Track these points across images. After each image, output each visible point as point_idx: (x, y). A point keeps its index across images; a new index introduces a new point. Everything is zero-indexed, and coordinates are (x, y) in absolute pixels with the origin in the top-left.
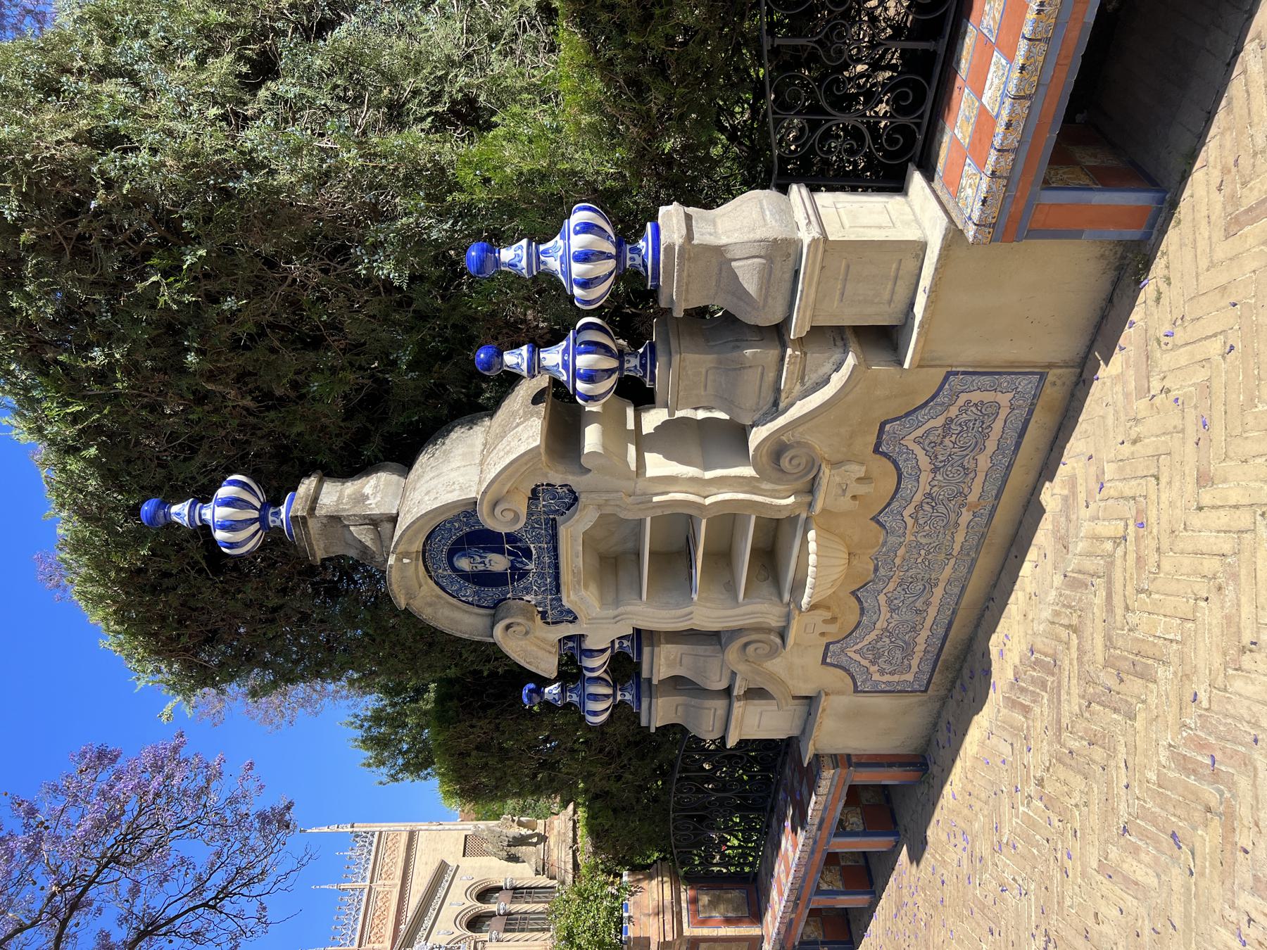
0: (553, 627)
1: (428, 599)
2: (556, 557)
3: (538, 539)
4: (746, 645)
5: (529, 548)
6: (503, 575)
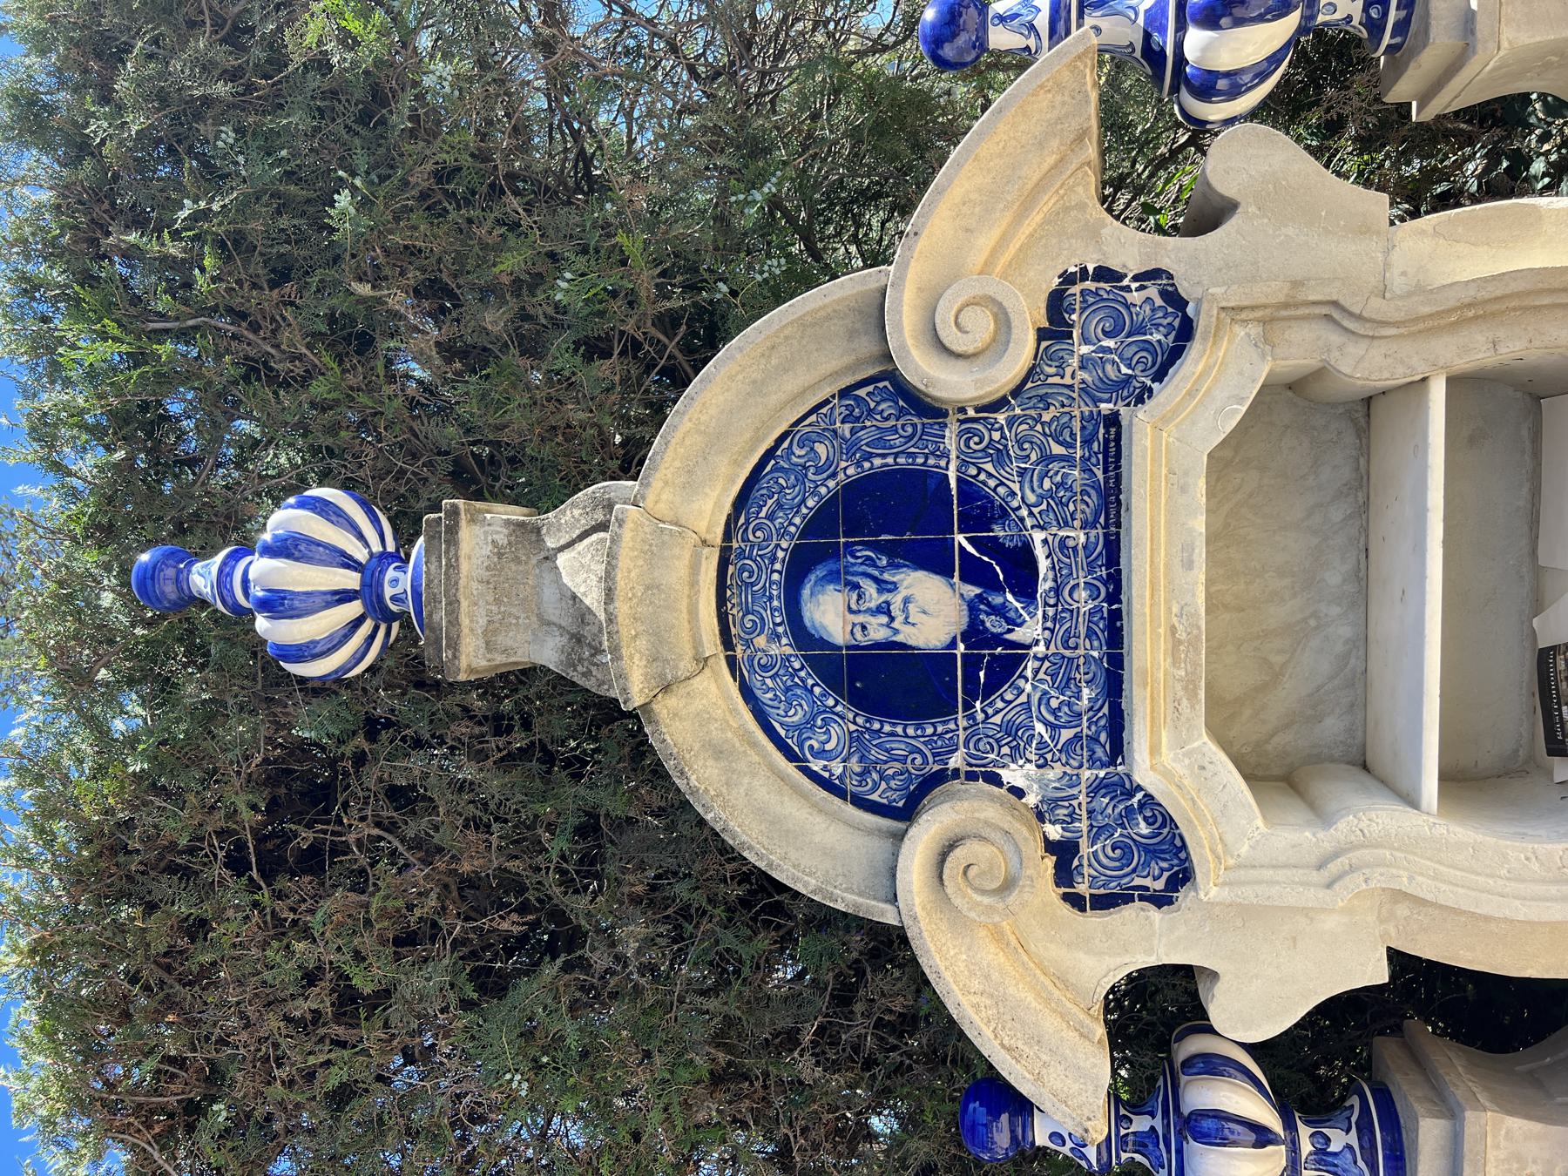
0: (1094, 920)
2: (1114, 586)
3: (1056, 507)
5: (1027, 549)
6: (939, 662)
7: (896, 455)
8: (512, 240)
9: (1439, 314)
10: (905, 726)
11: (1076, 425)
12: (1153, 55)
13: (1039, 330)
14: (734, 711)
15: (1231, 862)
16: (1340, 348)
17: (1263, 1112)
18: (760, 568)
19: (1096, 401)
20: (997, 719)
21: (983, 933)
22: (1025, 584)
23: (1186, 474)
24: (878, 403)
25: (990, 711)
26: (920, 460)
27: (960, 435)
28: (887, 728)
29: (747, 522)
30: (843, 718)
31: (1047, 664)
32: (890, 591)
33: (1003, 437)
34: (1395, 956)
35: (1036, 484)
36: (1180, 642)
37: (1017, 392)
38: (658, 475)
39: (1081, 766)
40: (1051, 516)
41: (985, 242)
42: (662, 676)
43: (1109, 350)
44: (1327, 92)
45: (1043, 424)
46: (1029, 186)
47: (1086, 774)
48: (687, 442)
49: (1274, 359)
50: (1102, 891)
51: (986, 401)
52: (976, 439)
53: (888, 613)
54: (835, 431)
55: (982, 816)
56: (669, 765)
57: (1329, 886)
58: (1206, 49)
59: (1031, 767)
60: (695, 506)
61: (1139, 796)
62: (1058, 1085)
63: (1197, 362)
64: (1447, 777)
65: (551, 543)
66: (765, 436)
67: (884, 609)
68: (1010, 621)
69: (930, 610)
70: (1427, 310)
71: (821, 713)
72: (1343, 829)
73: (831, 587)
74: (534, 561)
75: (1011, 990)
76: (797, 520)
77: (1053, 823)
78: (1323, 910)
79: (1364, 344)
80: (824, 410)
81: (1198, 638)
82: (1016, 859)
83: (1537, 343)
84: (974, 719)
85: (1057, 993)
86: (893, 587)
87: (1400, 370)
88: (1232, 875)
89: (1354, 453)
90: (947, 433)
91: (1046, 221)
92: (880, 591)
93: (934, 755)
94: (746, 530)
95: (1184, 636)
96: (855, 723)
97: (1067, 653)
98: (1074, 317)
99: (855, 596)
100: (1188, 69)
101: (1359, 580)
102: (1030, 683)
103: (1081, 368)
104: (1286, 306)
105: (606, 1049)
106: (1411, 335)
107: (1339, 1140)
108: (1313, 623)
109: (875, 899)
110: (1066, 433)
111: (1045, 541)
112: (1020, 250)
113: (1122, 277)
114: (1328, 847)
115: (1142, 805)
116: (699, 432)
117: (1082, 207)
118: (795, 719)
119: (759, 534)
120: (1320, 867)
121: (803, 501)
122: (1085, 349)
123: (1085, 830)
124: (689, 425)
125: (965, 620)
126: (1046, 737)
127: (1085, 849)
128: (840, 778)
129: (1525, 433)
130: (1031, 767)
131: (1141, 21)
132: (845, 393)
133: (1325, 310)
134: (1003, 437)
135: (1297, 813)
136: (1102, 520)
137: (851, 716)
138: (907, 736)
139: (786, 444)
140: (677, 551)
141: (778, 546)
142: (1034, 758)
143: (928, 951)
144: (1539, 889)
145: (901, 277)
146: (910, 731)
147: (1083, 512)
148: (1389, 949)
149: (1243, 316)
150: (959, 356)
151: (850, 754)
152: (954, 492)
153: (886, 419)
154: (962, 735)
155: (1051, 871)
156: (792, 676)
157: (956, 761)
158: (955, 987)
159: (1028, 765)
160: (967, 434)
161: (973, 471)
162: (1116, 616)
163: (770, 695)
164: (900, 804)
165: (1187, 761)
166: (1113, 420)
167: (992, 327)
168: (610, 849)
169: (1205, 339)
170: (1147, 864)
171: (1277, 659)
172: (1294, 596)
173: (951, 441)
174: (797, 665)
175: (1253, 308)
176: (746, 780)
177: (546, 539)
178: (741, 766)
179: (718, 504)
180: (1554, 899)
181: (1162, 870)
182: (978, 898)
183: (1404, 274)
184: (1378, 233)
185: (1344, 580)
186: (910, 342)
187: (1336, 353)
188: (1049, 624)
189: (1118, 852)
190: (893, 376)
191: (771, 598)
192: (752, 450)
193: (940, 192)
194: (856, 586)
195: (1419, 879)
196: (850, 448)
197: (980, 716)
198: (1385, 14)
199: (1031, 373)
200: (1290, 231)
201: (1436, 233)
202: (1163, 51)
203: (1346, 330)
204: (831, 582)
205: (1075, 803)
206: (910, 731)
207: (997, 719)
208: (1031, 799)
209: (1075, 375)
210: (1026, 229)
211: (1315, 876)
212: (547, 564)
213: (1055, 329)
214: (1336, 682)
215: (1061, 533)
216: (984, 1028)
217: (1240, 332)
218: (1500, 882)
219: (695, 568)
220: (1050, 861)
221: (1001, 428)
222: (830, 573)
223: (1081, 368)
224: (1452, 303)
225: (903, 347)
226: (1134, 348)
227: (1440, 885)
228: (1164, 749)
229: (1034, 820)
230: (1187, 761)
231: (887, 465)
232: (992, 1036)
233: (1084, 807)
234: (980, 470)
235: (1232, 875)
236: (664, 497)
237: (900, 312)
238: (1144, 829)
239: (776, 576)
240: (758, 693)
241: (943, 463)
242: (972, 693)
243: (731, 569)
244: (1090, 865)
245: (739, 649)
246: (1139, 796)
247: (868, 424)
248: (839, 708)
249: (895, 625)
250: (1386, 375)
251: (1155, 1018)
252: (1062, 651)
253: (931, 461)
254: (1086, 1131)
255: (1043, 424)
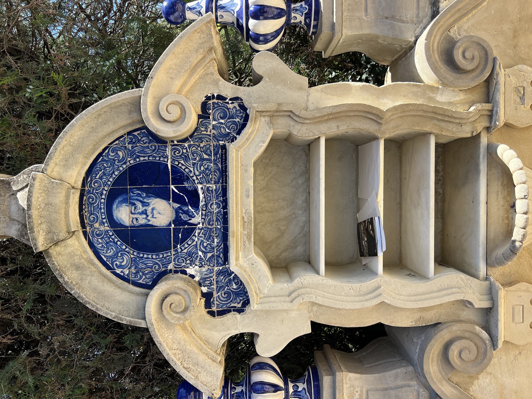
0: (218, 320)
1: (76, 260)
2: (225, 204)
3: (205, 177)
4: (447, 347)
5: (196, 191)
6: (165, 231)
7: (149, 157)
8: (9, 73)
9: (322, 117)
10: (152, 255)
11: (212, 149)
12: (240, 26)
13: (199, 115)
14: (85, 252)
15: (262, 296)
16: (293, 126)
17: (277, 381)
18: (96, 198)
19: (218, 141)
20: (185, 251)
21: (178, 327)
22: (195, 203)
23: (247, 166)
24: (142, 138)
25: (183, 248)
26: (158, 159)
27: (172, 150)
28: (145, 256)
29: (91, 180)
30: (128, 253)
31: (203, 231)
32: (147, 206)
33: (187, 151)
34: (313, 324)
35: (198, 168)
36: (245, 222)
37: (191, 136)
38: (52, 161)
39: (214, 266)
40: (204, 179)
41: (178, 83)
42: (52, 239)
43: (222, 123)
44: (299, 47)
45: (201, 147)
46: (193, 65)
47: (216, 268)
48: (65, 149)
49: (273, 129)
50: (221, 309)
51: (180, 138)
52: (178, 152)
53: (146, 214)
54: (125, 147)
55: (176, 285)
56: (56, 273)
57: (292, 302)
58: (254, 26)
59: (197, 267)
60: (69, 173)
61: (233, 275)
62: (204, 379)
63: (249, 129)
64: (328, 264)
65: (14, 188)
66: (98, 148)
67: (145, 213)
68: (190, 216)
69: (161, 213)
70: (318, 115)
71: (120, 251)
72: (297, 282)
73: (124, 204)
74: (8, 195)
75: (188, 347)
76: (111, 180)
77: (204, 287)
78: (291, 310)
79: (300, 125)
80: (121, 139)
81: (251, 220)
82: (189, 300)
83: (350, 127)
84: (177, 251)
85: (205, 347)
86: (148, 204)
87: (311, 134)
88: (262, 300)
89: (305, 162)
90: (167, 149)
91: (200, 78)
92: (143, 206)
93: (163, 265)
94: (91, 183)
95: (247, 220)
96: (133, 255)
97: (210, 227)
98: (210, 111)
99: (133, 208)
100: (250, 32)
101: (307, 202)
102: (197, 238)
103: (213, 129)
104: (277, 111)
105: (46, 385)
106: (315, 123)
107: (301, 386)
108: (293, 216)
109: (138, 318)
110: (209, 151)
111: (202, 188)
112: (192, 87)
113: (226, 99)
114: (292, 289)
115: (234, 278)
116: (70, 145)
117: (212, 74)
118: (110, 254)
119: (96, 184)
120: (289, 295)
121: (114, 172)
122: (214, 123)
123: (215, 288)
124: (65, 142)
125: (174, 216)
126: (202, 256)
127: (215, 295)
128: (128, 275)
129: (354, 156)
130: (197, 267)
131: (235, 15)
132: (129, 133)
133: (288, 114)
134: (187, 151)
135: (286, 277)
136: (221, 181)
137: (132, 252)
138: (153, 258)
139: (107, 151)
140: (59, 190)
141: (103, 189)
142: (198, 264)
143: (157, 336)
144: (353, 298)
145: (146, 94)
146: (154, 257)
147: (214, 178)
148: (311, 322)
149: (264, 114)
150: (168, 122)
151: (131, 266)
152: (170, 170)
153: (145, 143)
154: (173, 257)
155: (203, 303)
156: (109, 238)
157: (171, 267)
158: (167, 348)
159: (196, 267)
160: (174, 150)
161: (177, 163)
162: (226, 214)
163: (100, 245)
164: (150, 283)
165: (248, 262)
166: (224, 147)
167: (179, 112)
168: (49, 308)
169: (251, 121)
170: (236, 299)
171: (283, 228)
172: (288, 207)
173: (169, 152)
174: (111, 234)
175: (267, 112)
176: (89, 278)
177: (13, 187)
178: (88, 272)
179: (79, 173)
180: (357, 302)
181: (241, 300)
182: (175, 315)
183: (313, 103)
184: (305, 90)
185: (303, 202)
186: (150, 116)
187: (292, 128)
188: (203, 217)
189: (226, 295)
190: (145, 128)
191: (101, 209)
192: (93, 153)
193: (161, 64)
194: (134, 204)
195: (318, 298)
196: (131, 153)
197: (179, 250)
198: (311, 21)
199: (196, 130)
200: (279, 87)
201: (322, 91)
202: (243, 25)
203: (295, 120)
204: (124, 203)
205: (212, 279)
206: (154, 257)
207: (185, 251)
208: (197, 279)
209: (211, 131)
210: (193, 80)
211: (288, 299)
212: (13, 196)
213: (204, 115)
214: (301, 235)
215: (207, 185)
216: (177, 362)
217: (263, 119)
218: (342, 297)
219: (67, 197)
220: (203, 300)
221: (186, 148)
222: (124, 199)
223: (213, 129)
224: (325, 113)
225: (147, 117)
226: (230, 123)
227: (324, 299)
228: (240, 259)
229: (198, 286)
230: (248, 262)
231: (145, 160)
232: (180, 364)
233: (215, 280)
234: (179, 163)
235: (262, 300)
236: (55, 170)
237: (146, 105)
238: (235, 286)
239: (103, 201)
240: (96, 245)
241: (166, 160)
242: (176, 242)
243: (85, 198)
244: (217, 300)
245: (88, 228)
246: (233, 275)
247: (138, 145)
248: (127, 249)
249: (149, 218)
250: (307, 136)
251: (240, 353)
252: (208, 226)
253: (162, 159)
254: (213, 394)
255: (201, 147)
